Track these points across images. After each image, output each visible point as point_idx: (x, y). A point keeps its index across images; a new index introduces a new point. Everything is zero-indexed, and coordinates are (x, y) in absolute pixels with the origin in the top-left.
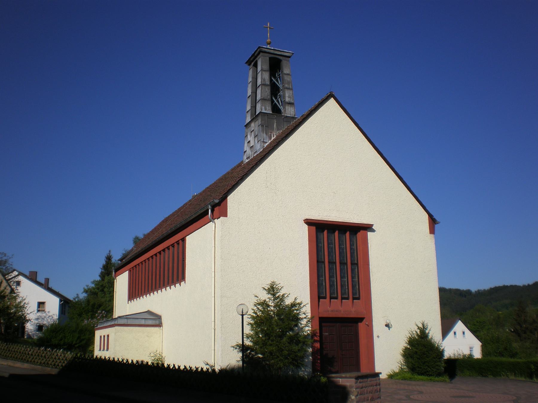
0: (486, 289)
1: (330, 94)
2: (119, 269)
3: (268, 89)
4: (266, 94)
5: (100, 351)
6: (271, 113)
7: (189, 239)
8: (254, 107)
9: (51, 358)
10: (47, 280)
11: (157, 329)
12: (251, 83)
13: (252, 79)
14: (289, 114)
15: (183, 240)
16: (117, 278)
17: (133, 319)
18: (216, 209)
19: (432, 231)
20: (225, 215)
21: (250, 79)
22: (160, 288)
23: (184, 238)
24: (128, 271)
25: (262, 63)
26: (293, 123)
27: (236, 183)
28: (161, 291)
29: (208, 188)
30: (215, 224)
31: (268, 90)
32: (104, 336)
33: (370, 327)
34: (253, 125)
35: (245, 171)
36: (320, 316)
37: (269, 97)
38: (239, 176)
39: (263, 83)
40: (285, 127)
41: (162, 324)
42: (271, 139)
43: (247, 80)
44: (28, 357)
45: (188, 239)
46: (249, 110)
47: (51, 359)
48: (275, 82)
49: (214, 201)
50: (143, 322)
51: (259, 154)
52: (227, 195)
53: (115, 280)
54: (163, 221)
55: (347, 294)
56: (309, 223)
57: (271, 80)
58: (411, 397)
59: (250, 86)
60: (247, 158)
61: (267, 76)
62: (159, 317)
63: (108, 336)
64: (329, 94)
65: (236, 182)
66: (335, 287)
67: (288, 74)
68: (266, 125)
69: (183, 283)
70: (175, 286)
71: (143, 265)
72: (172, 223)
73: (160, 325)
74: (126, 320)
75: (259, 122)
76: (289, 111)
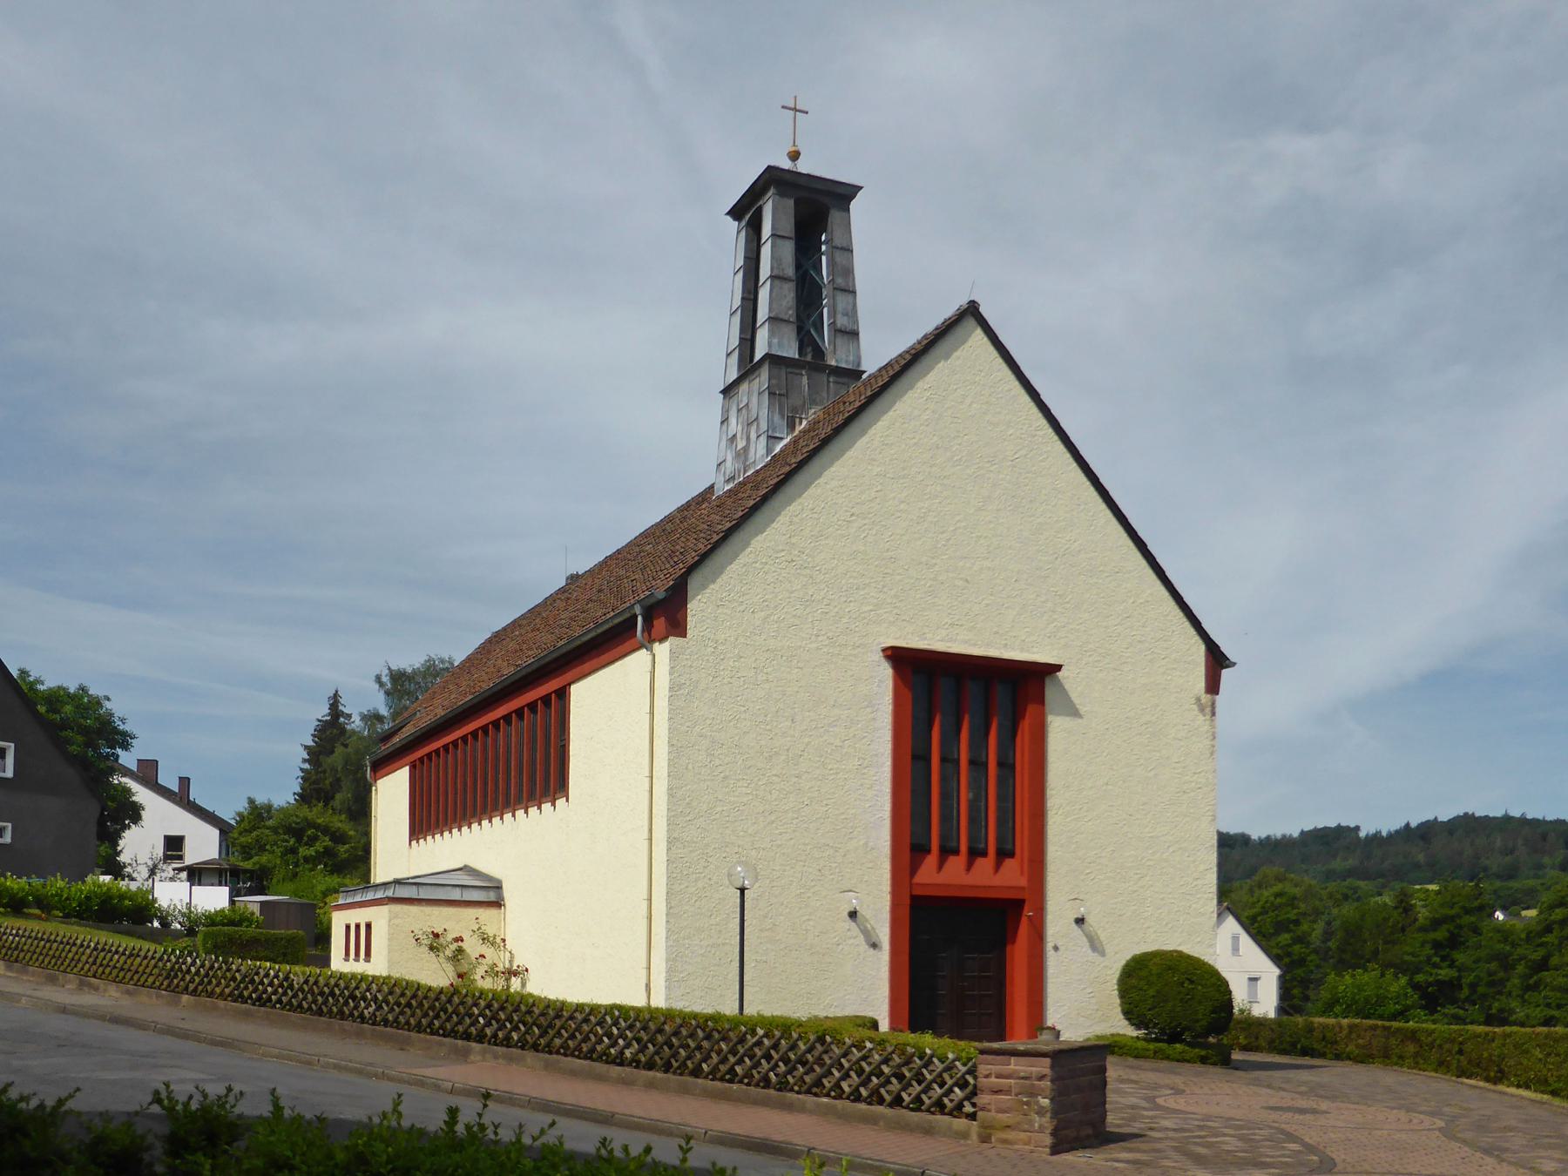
0: (1231, 833)
4: (784, 303)
10: (185, 782)
13: (745, 262)
15: (563, 694)
16: (378, 782)
17: (433, 887)
18: (660, 624)
20: (683, 634)
23: (565, 686)
27: (709, 547)
28: (514, 816)
31: (789, 293)
32: (358, 926)
34: (744, 387)
36: (918, 892)
37: (790, 312)
39: (776, 272)
42: (791, 427)
44: (188, 978)
46: (734, 350)
50: (456, 895)
51: (761, 469)
53: (374, 788)
56: (897, 656)
57: (798, 266)
60: (728, 481)
61: (788, 249)
62: (498, 887)
63: (369, 926)
65: (710, 544)
68: (782, 392)
69: (561, 802)
75: (763, 378)
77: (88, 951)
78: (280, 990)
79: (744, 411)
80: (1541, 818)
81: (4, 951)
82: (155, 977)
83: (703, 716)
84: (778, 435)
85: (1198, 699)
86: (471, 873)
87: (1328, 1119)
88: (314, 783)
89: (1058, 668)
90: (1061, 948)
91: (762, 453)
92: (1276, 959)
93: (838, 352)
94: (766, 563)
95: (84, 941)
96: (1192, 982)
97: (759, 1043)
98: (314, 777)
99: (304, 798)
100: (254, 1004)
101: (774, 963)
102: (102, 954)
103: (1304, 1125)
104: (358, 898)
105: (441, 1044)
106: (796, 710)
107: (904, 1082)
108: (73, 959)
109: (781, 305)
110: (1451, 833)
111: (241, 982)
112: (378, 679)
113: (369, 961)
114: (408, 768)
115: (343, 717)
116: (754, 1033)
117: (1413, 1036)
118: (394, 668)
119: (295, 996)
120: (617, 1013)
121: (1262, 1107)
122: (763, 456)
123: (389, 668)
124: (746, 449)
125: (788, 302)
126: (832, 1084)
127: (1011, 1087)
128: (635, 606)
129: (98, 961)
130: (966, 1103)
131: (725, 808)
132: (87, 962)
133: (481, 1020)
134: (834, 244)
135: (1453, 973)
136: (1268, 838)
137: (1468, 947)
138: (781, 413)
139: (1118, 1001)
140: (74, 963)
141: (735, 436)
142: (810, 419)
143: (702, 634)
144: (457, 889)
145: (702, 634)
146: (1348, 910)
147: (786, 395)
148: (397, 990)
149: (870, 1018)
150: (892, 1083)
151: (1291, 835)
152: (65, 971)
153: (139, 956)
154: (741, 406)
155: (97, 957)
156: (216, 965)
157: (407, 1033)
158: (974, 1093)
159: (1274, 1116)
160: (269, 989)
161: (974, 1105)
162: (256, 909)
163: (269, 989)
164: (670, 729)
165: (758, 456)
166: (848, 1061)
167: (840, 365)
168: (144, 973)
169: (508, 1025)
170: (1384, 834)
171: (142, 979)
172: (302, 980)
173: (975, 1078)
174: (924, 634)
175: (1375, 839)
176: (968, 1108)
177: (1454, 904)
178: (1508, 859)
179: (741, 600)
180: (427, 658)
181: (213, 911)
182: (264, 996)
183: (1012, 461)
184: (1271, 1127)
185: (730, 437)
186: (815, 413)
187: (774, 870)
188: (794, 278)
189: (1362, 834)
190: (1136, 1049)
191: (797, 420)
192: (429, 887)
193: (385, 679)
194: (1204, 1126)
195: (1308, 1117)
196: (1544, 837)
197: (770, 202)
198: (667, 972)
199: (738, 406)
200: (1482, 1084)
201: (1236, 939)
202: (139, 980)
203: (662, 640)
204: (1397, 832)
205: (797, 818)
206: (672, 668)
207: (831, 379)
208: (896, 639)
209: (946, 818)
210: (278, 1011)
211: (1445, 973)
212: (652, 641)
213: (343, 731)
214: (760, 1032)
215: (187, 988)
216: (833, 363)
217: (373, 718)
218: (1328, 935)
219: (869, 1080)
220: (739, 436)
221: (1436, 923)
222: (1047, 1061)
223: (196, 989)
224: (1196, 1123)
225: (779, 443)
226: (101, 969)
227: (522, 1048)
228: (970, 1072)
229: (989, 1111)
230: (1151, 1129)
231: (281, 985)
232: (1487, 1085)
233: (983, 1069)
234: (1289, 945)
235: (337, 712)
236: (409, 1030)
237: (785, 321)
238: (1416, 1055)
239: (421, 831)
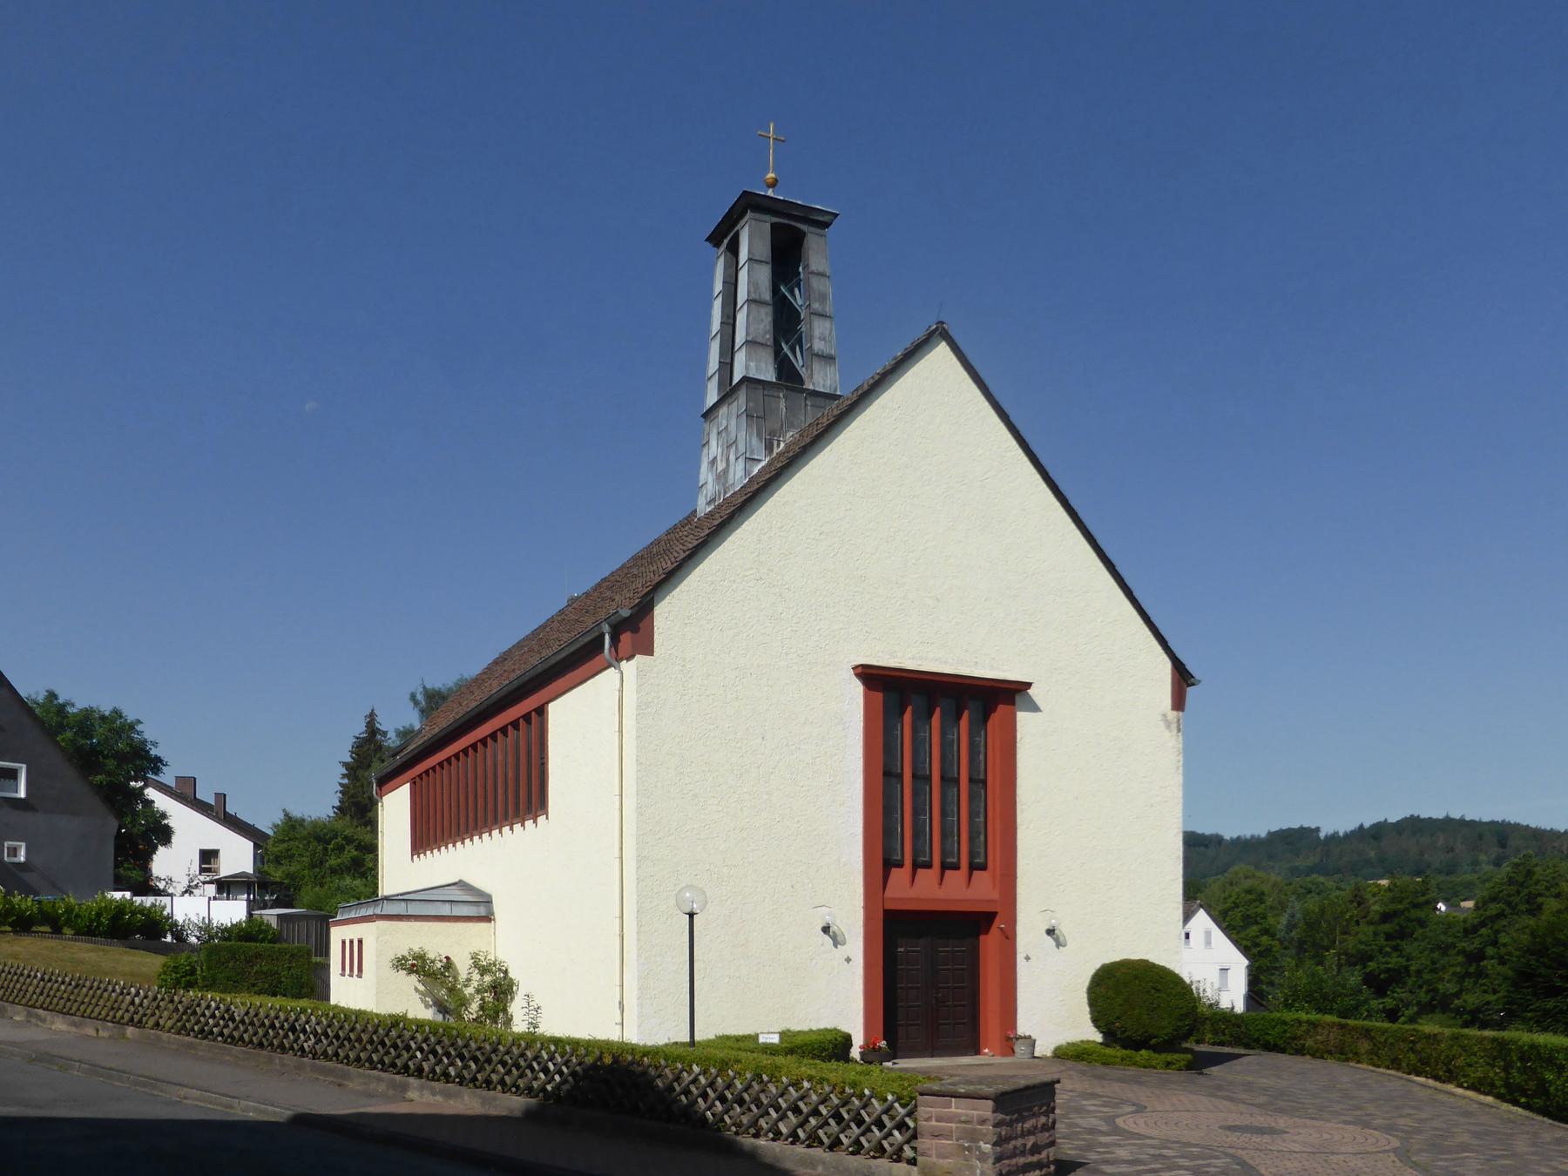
1: (937, 329)
2: (387, 780)
3: (766, 314)
4: (762, 326)
5: (344, 976)
6: (774, 380)
7: (555, 710)
8: (727, 365)
9: (191, 1015)
10: (221, 798)
11: (483, 925)
12: (716, 378)
14: (821, 386)
15: (541, 711)
18: (626, 638)
19: (1179, 703)
20: (648, 650)
21: (718, 286)
22: (497, 826)
24: (409, 784)
25: (752, 239)
26: (834, 408)
27: (675, 564)
29: (605, 580)
30: (622, 673)
31: (765, 317)
32: (351, 942)
33: (1010, 937)
34: (723, 410)
35: (702, 535)
36: (889, 906)
37: (768, 336)
38: (685, 548)
39: (753, 296)
40: (809, 416)
41: (493, 914)
43: (712, 289)
45: (553, 708)
47: (192, 1018)
48: (786, 293)
49: (618, 612)
50: (445, 910)
51: (739, 490)
52: (653, 597)
53: (380, 804)
54: (496, 662)
55: (956, 855)
56: (871, 677)
57: (775, 290)
58: (1119, 1121)
59: (718, 306)
60: (709, 503)
61: (764, 274)
62: (486, 900)
63: (360, 942)
64: (934, 327)
66: (926, 837)
67: (822, 275)
68: (759, 414)
69: (541, 819)
70: (523, 825)
71: (452, 768)
72: (516, 667)
73: (488, 918)
74: (403, 904)
75: (741, 401)
76: (821, 379)
77: (35, 982)
78: (221, 1022)
79: (724, 434)
80: (1477, 819)
81: (3, 975)
82: (100, 1007)
83: (671, 734)
84: (756, 457)
85: (1164, 715)
86: (464, 888)
87: (1284, 1141)
88: (352, 796)
89: (1029, 685)
90: (1033, 959)
91: (740, 475)
92: (1245, 950)
93: (815, 377)
94: (734, 581)
95: (31, 970)
96: (1158, 990)
97: (695, 1081)
98: (352, 792)
99: (341, 810)
100: (196, 1037)
101: (748, 979)
102: (49, 985)
103: (1261, 1150)
104: (352, 915)
105: (379, 1079)
106: (766, 728)
107: (843, 1125)
108: (21, 990)
109: (758, 329)
110: (1400, 833)
111: (183, 1014)
112: (413, 697)
113: (361, 977)
114: (409, 784)
115: (380, 734)
116: (690, 1072)
117: (1367, 1033)
118: (429, 686)
119: (236, 1028)
120: (553, 1048)
121: (1220, 1127)
122: (741, 477)
123: (424, 687)
124: (726, 471)
125: (765, 326)
126: (769, 1125)
127: (952, 1132)
128: (603, 625)
129: (46, 991)
130: (906, 1148)
131: (695, 826)
132: (34, 993)
133: (418, 1054)
134: (810, 270)
135: (1403, 961)
136: (1239, 838)
137: (1416, 939)
138: (759, 435)
139: (1088, 1009)
140: (22, 993)
141: (715, 458)
142: (787, 442)
143: (669, 652)
144: (447, 904)
145: (669, 652)
146: (1312, 904)
147: (764, 418)
148: (336, 1023)
149: (845, 1033)
150: (829, 1125)
151: (1259, 836)
152: (13, 1002)
153: (84, 986)
154: (721, 429)
155: (44, 988)
156: (159, 996)
157: (346, 1067)
158: (914, 1137)
159: (1233, 1138)
160: (211, 1021)
161: (914, 1149)
162: (274, 923)
163: (211, 1021)
164: (638, 747)
165: (736, 478)
166: (785, 1101)
167: (817, 389)
168: (90, 1003)
169: (445, 1060)
170: (1341, 834)
171: (88, 1011)
172: (243, 1013)
173: (915, 1120)
174: (895, 652)
175: (1333, 838)
176: (908, 1152)
177: (1403, 899)
178: (1451, 855)
179: (709, 617)
180: (460, 677)
181: (229, 925)
182: (206, 1028)
183: (982, 481)
184: (1228, 1155)
185: (711, 459)
186: (793, 436)
187: (745, 886)
188: (771, 303)
189: (1322, 835)
190: (1104, 1055)
191: (775, 443)
192: (418, 902)
193: (420, 697)
194: (1160, 1155)
195: (1267, 1138)
196: (1481, 837)
197: (746, 229)
198: (638, 990)
199: (718, 428)
200: (1431, 1082)
201: (1208, 934)
202: (85, 1011)
203: (629, 658)
204: (1352, 832)
205: (769, 835)
206: (639, 686)
207: (809, 403)
208: (867, 656)
209: (917, 833)
210: (221, 1045)
211: (1395, 961)
212: (619, 660)
213: (379, 748)
214: (696, 1069)
215: (132, 1019)
216: (811, 387)
217: (406, 734)
218: (1291, 926)
219: (806, 1121)
220: (719, 458)
221: (1386, 917)
222: (990, 1103)
223: (140, 1021)
224: (1152, 1151)
225: (757, 465)
226: (48, 1000)
227: (460, 1084)
228: (910, 1114)
229: (930, 1156)
230: (1107, 1162)
231: (223, 1018)
232: (1438, 1084)
233: (922, 1111)
234: (1257, 936)
235: (373, 730)
236: (347, 1064)
237: (762, 344)
238: (1370, 1053)
239: (421, 847)
